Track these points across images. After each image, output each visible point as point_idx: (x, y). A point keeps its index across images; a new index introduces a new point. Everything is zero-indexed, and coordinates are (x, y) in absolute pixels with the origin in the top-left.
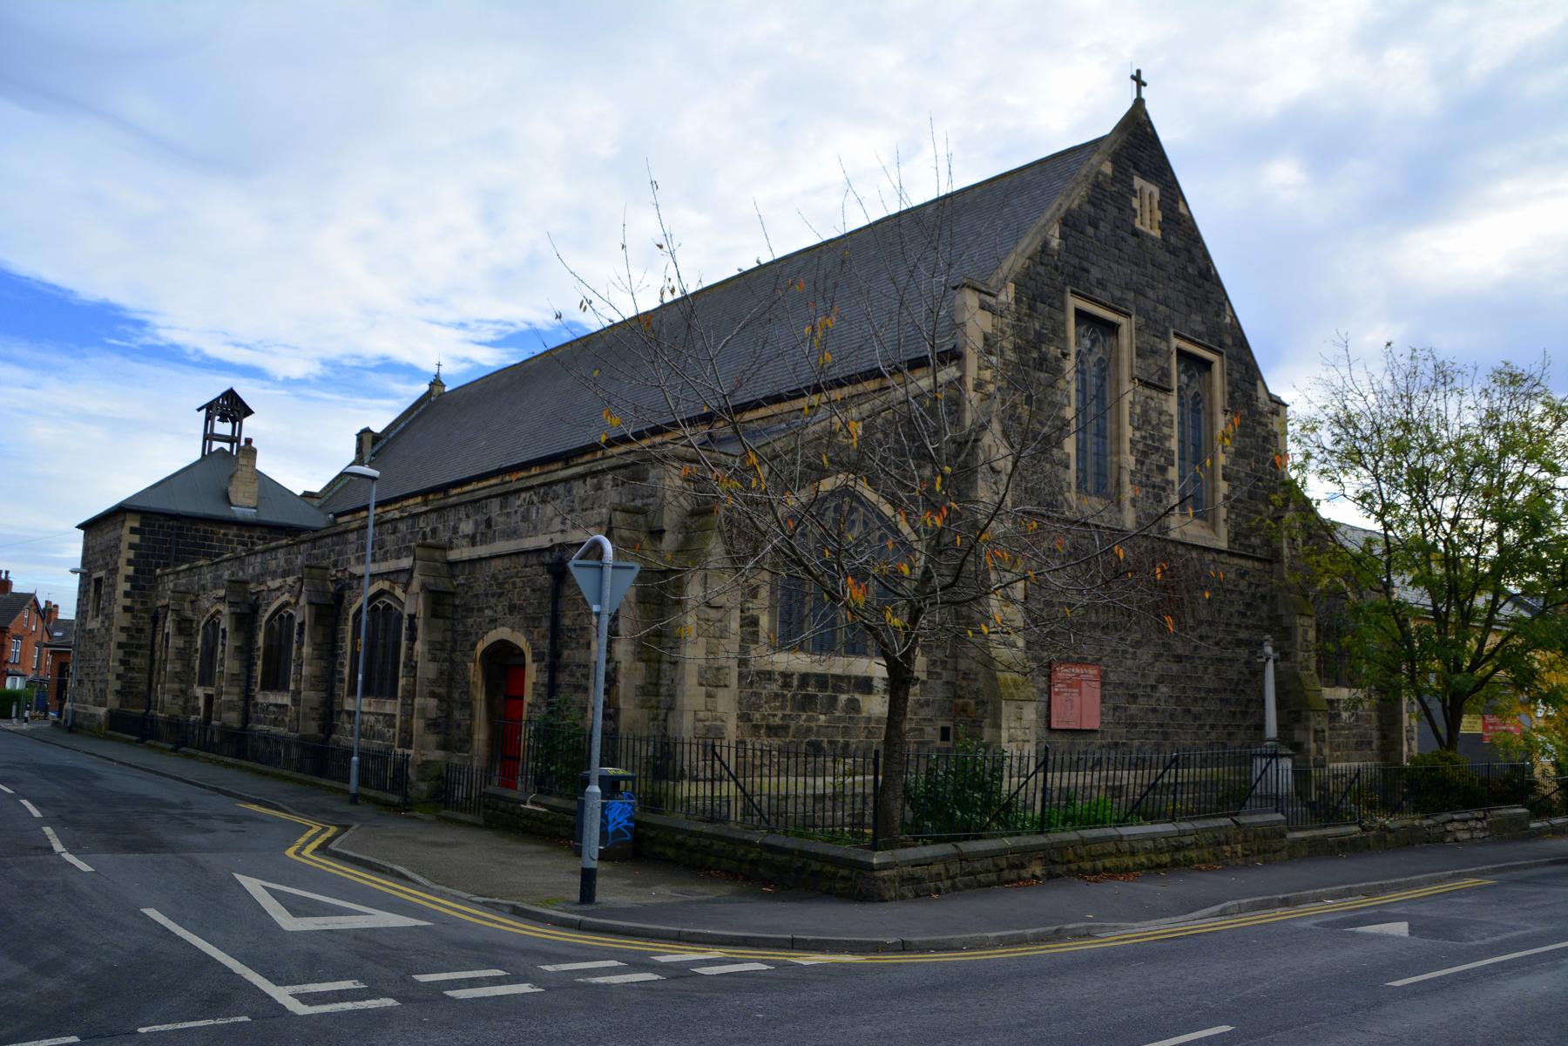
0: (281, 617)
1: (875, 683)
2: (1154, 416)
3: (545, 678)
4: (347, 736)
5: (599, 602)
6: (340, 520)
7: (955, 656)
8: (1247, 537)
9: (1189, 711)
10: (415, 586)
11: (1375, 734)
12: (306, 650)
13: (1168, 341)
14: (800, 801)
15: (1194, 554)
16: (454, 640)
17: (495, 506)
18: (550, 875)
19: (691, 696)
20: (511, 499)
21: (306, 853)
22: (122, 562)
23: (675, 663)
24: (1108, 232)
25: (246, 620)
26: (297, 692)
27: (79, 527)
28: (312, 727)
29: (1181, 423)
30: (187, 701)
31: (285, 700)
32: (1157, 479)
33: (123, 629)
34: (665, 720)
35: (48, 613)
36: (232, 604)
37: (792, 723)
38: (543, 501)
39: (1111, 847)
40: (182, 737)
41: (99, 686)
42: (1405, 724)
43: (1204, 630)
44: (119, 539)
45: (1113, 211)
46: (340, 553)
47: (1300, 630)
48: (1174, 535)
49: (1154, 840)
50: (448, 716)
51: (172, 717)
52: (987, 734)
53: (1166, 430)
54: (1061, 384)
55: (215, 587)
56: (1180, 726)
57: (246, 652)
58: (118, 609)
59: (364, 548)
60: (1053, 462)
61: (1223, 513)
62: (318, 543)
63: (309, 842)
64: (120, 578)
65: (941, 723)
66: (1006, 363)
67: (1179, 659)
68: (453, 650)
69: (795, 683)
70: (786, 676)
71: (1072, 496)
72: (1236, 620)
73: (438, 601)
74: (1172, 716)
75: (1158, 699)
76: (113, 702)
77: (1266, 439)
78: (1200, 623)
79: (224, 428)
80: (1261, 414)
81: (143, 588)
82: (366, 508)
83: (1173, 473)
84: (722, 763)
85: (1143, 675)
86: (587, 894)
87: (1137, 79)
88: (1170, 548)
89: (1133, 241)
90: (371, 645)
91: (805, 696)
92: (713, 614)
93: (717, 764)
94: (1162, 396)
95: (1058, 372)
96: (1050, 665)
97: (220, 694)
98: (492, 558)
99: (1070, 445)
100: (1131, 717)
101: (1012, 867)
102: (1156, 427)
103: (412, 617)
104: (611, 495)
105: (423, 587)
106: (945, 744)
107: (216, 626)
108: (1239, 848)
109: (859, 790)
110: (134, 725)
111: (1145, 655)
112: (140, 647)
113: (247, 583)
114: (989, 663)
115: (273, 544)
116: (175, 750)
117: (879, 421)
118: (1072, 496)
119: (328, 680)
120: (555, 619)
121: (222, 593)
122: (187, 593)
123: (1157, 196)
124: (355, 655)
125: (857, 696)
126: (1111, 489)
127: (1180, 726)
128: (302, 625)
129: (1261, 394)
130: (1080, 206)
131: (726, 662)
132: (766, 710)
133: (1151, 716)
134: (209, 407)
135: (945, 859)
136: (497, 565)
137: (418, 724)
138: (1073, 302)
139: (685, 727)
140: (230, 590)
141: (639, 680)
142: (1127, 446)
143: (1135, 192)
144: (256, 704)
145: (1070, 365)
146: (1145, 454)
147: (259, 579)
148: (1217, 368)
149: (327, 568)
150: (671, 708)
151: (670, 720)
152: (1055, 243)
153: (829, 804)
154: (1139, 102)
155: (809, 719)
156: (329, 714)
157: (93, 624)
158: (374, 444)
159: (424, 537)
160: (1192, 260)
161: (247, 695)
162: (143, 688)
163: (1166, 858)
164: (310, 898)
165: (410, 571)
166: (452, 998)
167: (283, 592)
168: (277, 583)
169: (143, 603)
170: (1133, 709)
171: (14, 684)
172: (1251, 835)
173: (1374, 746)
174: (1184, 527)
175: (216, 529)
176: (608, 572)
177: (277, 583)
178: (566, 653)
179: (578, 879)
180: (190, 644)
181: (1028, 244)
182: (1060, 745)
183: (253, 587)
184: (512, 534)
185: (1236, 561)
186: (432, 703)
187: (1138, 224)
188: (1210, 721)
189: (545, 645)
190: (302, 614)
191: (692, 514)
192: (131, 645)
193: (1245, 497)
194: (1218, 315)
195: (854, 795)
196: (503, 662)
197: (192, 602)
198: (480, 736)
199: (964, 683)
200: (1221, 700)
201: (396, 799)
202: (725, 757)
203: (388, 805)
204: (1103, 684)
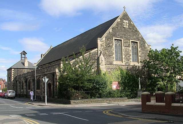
22: (12, 75)
25: (26, 82)
32: (128, 58)
33: (13, 83)
36: (24, 80)
54: (112, 48)
79: (23, 56)
83: (131, 57)
94: (129, 48)
99: (114, 56)
116: (19, 98)
136: (49, 74)
138: (114, 38)
145: (114, 46)
160: (134, 29)
166: (149, 105)
184: (50, 71)
187: (124, 26)
190: (31, 81)
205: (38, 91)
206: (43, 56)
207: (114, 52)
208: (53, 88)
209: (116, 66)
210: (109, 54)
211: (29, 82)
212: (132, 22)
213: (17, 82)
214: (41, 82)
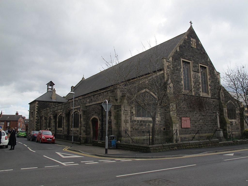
2: (197, 77)
3: (101, 123)
4: (72, 134)
5: (106, 110)
6: (69, 101)
7: (165, 117)
8: (214, 95)
9: (206, 124)
10: (81, 110)
11: (240, 127)
12: (65, 121)
13: (198, 64)
14: (141, 140)
15: (205, 99)
16: (87, 118)
18: (103, 151)
19: (123, 124)
21: (66, 149)
22: (36, 109)
23: (120, 119)
24: (188, 49)
25: (55, 117)
28: (66, 133)
29: (202, 77)
31: (62, 129)
32: (198, 87)
34: (119, 128)
35: (24, 118)
36: (53, 115)
37: (139, 128)
38: (100, 96)
39: (188, 144)
41: (33, 129)
42: (245, 125)
43: (207, 111)
44: (35, 105)
45: (188, 44)
46: (69, 106)
47: (224, 110)
48: (201, 95)
52: (171, 129)
55: (50, 112)
56: (204, 127)
57: (55, 122)
58: (35, 116)
59: (73, 105)
61: (210, 92)
63: (66, 148)
64: (36, 111)
67: (203, 116)
68: (87, 120)
69: (140, 122)
71: (183, 90)
73: (84, 112)
74: (203, 125)
77: (216, 79)
78: (207, 110)
79: (50, 87)
80: (215, 75)
81: (39, 113)
82: (73, 99)
83: (201, 86)
84: (127, 134)
85: (197, 119)
86: (106, 152)
87: (191, 23)
88: (201, 98)
89: (191, 49)
90: (74, 120)
91: (141, 124)
92: (126, 112)
93: (126, 134)
94: (198, 73)
97: (52, 129)
98: (92, 105)
99: (183, 82)
102: (197, 78)
103: (80, 115)
104: (110, 94)
106: (164, 131)
107: (50, 118)
108: (210, 145)
111: (197, 115)
112: (39, 122)
115: (59, 105)
117: (151, 80)
118: (183, 90)
119: (68, 125)
120: (102, 114)
121: (51, 113)
123: (195, 41)
124: (72, 121)
125: (149, 124)
127: (204, 127)
128: (64, 117)
129: (215, 71)
131: (129, 119)
132: (135, 126)
134: (48, 84)
135: (161, 146)
136: (93, 106)
137: (82, 131)
138: (182, 59)
142: (192, 82)
143: (191, 41)
145: (182, 70)
147: (57, 110)
148: (207, 68)
151: (120, 128)
152: (178, 50)
153: (145, 141)
154: (191, 26)
155: (142, 127)
156: (69, 131)
157: (31, 119)
158: (74, 89)
159: (82, 102)
160: (202, 51)
161: (56, 129)
163: (198, 146)
164: (66, 157)
165: (80, 108)
167: (61, 113)
170: (196, 124)
173: (240, 129)
174: (202, 94)
178: (104, 119)
179: (105, 150)
181: (174, 51)
182: (184, 130)
184: (95, 101)
185: (212, 99)
186: (84, 128)
187: (192, 46)
188: (209, 126)
189: (101, 118)
190: (64, 115)
191: (122, 96)
192: (37, 122)
193: (213, 89)
194: (207, 59)
196: (95, 121)
197: (47, 115)
198: (92, 133)
199: (167, 121)
202: (129, 134)
203: (78, 144)
204: (190, 120)
207: (182, 77)
208: (102, 125)
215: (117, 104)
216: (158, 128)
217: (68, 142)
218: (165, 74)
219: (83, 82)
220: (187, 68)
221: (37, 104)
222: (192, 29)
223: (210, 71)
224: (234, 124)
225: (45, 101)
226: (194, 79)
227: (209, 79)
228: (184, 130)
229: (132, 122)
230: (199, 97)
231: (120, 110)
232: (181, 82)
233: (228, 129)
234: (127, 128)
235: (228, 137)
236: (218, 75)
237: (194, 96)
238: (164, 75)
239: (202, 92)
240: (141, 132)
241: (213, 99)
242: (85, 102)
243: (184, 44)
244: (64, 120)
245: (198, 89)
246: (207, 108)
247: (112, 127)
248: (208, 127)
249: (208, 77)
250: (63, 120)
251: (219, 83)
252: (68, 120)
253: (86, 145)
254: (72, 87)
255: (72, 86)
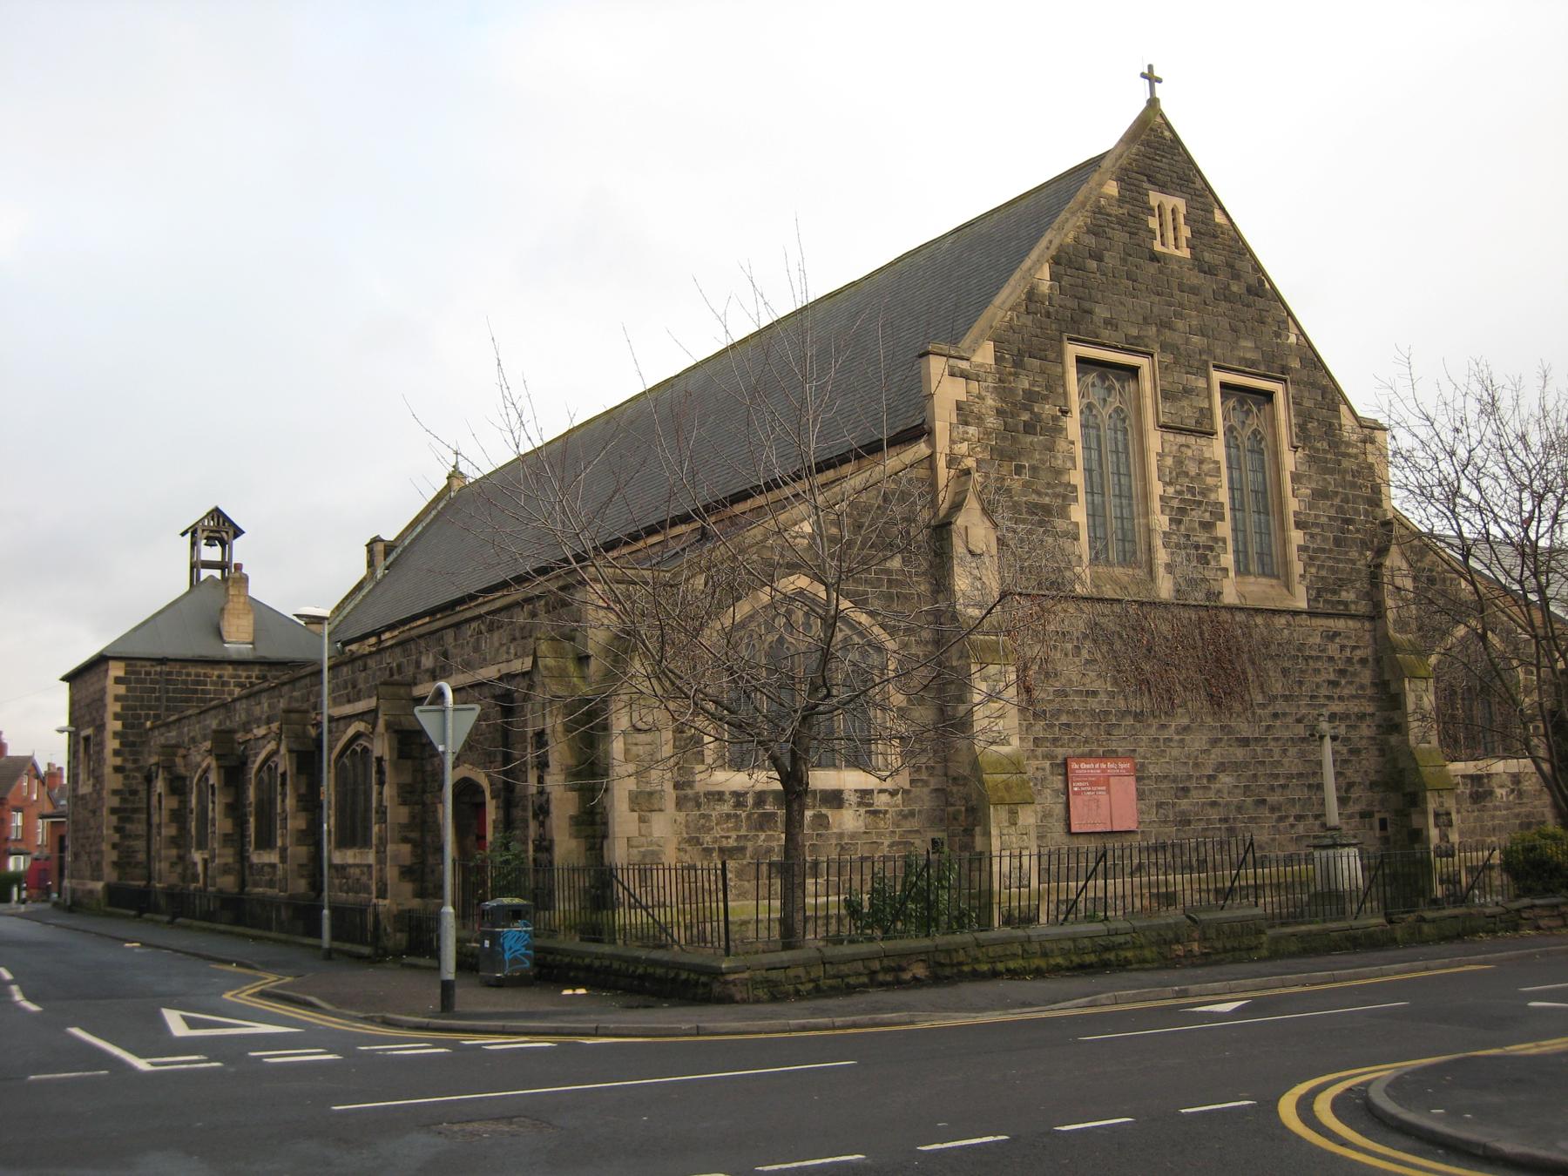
0: (270, 768)
1: (845, 796)
2: (1193, 469)
5: (444, 742)
13: (1208, 378)
15: (1259, 620)
17: (449, 636)
20: (465, 627)
22: (109, 717)
24: (1128, 260)
26: (284, 850)
27: (63, 679)
30: (185, 869)
32: (1202, 538)
33: (115, 792)
37: (749, 844)
38: (490, 630)
40: (180, 907)
41: (95, 858)
43: (1280, 706)
44: (103, 691)
45: (1120, 236)
48: (1230, 596)
49: (1074, 940)
50: (423, 863)
51: (172, 887)
53: (1210, 481)
54: (1061, 445)
56: (1252, 820)
57: (235, 810)
60: (1056, 535)
61: (1298, 568)
62: (298, 685)
64: (108, 734)
65: (930, 835)
66: (987, 433)
67: (1245, 742)
68: (424, 792)
69: (750, 801)
70: (739, 797)
72: (1324, 691)
74: (1239, 809)
75: (1219, 791)
76: (110, 875)
79: (212, 553)
80: (1348, 444)
81: (133, 744)
83: (1224, 529)
85: (1196, 765)
86: (447, 1004)
87: (1151, 77)
89: (1152, 268)
94: (1203, 441)
95: (1057, 430)
96: (1065, 764)
97: (213, 857)
99: (1079, 513)
100: (1183, 813)
101: (887, 970)
105: (388, 726)
109: (833, 911)
110: (132, 901)
111: (1198, 741)
112: (135, 810)
113: (233, 731)
114: (975, 765)
122: (178, 746)
123: (1182, 209)
125: (824, 811)
126: (1142, 556)
127: (1252, 820)
128: (284, 775)
130: (1076, 239)
132: (718, 832)
133: (1209, 810)
134: (193, 531)
138: (1073, 351)
139: (619, 853)
140: (214, 741)
141: (572, 810)
142: (1156, 505)
144: (251, 866)
145: (1073, 425)
146: (1182, 511)
149: (307, 712)
150: (605, 836)
154: (1153, 103)
160: (1236, 276)
162: (141, 857)
168: (261, 731)
169: (135, 761)
170: (1184, 804)
171: (15, 864)
172: (1212, 933)
175: (208, 671)
176: (450, 714)
177: (261, 731)
179: (439, 991)
180: (184, 803)
183: (240, 737)
186: (406, 848)
187: (1158, 247)
188: (1296, 810)
190: (284, 763)
192: (125, 810)
194: (1278, 335)
195: (827, 917)
197: (184, 757)
200: (1310, 786)
201: (366, 950)
203: (360, 957)
204: (1139, 779)
205: (349, 857)
206: (379, 558)
207: (1077, 478)
209: (1099, 607)
210: (1034, 498)
211: (260, 782)
212: (1217, 213)
213: (149, 780)
214: (380, 772)
215: (585, 690)
216: (887, 843)
217: (269, 939)
218: (941, 463)
219: (457, 506)
220: (1118, 410)
221: (118, 680)
222: (1159, 120)
223: (1303, 420)
224: (1499, 792)
225: (176, 660)
226: (1170, 483)
227: (1296, 478)
228: (1109, 846)
229: (698, 805)
230: (1213, 605)
231: (605, 727)
232: (1063, 513)
233: (1434, 833)
234: (651, 843)
235: (1439, 891)
236: (1373, 442)
237: (1165, 605)
238: (933, 468)
239: (1232, 574)
240: (764, 868)
241: (1328, 615)
242: (410, 671)
243: (1090, 241)
244: (284, 796)
245: (1205, 554)
246: (1278, 687)
247: (551, 841)
248: (1281, 819)
249: (1290, 461)
250: (279, 798)
251: (1375, 498)
252: (310, 803)
253: (404, 966)
254: (371, 546)
255: (376, 540)
